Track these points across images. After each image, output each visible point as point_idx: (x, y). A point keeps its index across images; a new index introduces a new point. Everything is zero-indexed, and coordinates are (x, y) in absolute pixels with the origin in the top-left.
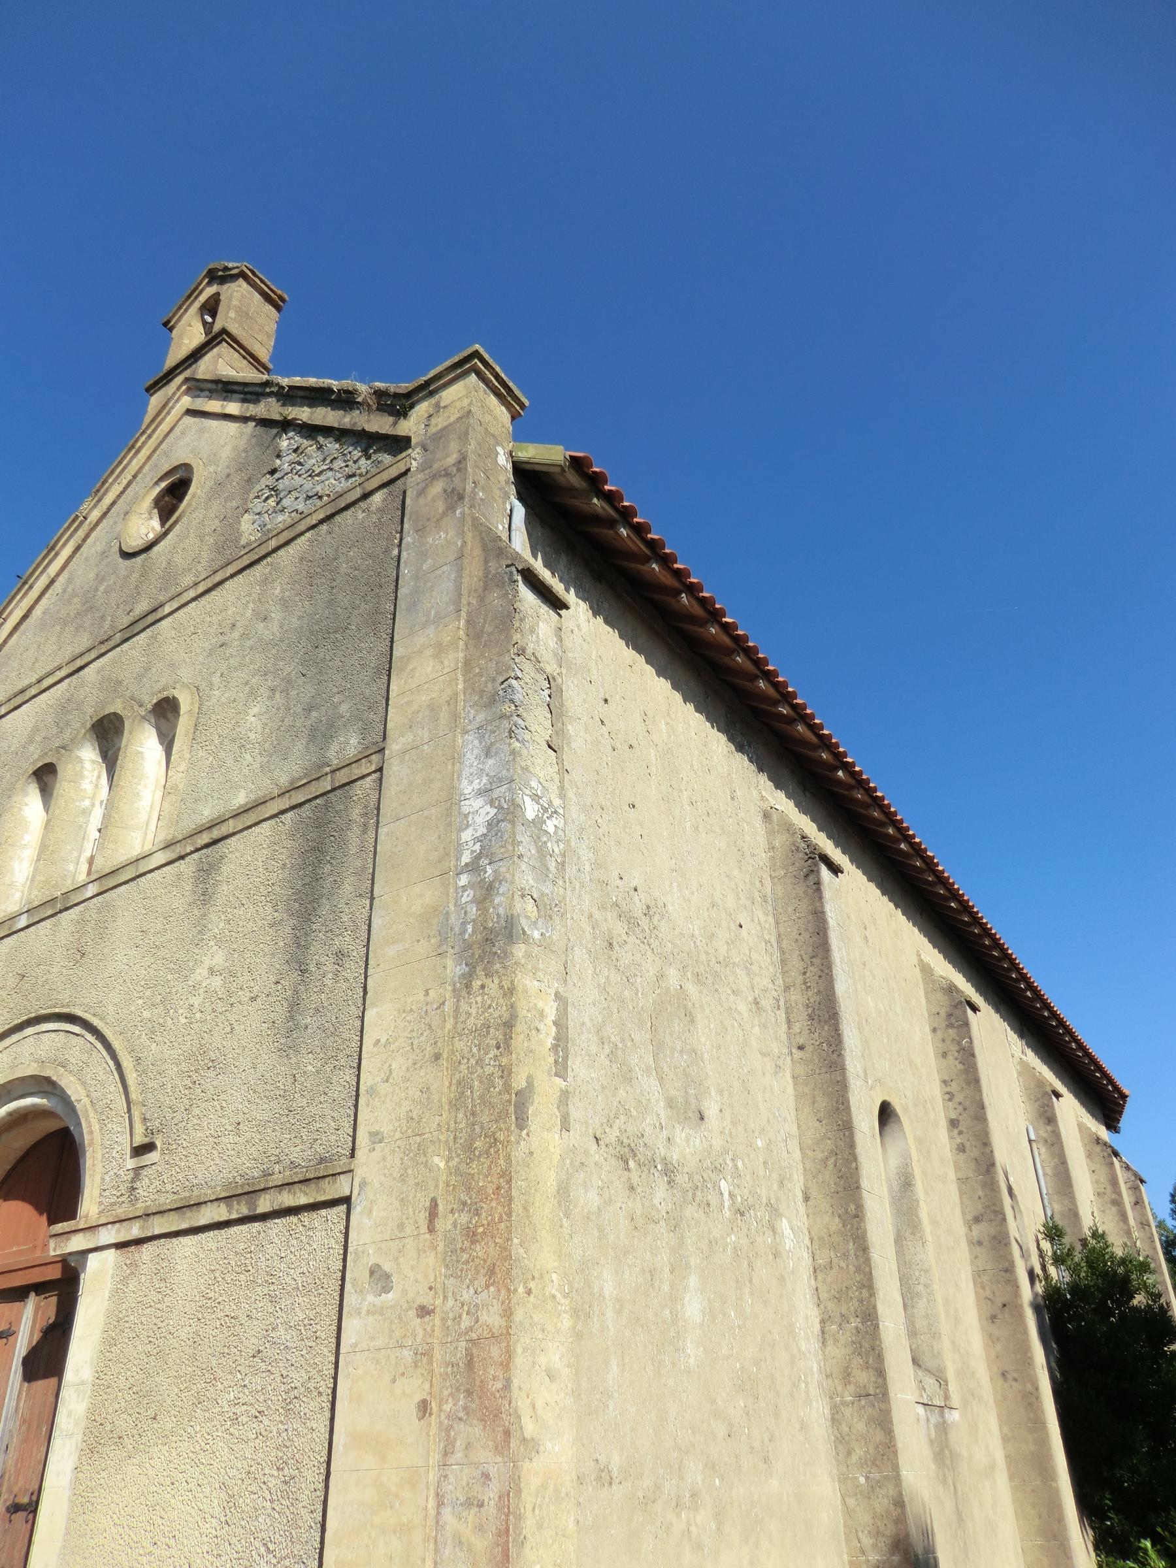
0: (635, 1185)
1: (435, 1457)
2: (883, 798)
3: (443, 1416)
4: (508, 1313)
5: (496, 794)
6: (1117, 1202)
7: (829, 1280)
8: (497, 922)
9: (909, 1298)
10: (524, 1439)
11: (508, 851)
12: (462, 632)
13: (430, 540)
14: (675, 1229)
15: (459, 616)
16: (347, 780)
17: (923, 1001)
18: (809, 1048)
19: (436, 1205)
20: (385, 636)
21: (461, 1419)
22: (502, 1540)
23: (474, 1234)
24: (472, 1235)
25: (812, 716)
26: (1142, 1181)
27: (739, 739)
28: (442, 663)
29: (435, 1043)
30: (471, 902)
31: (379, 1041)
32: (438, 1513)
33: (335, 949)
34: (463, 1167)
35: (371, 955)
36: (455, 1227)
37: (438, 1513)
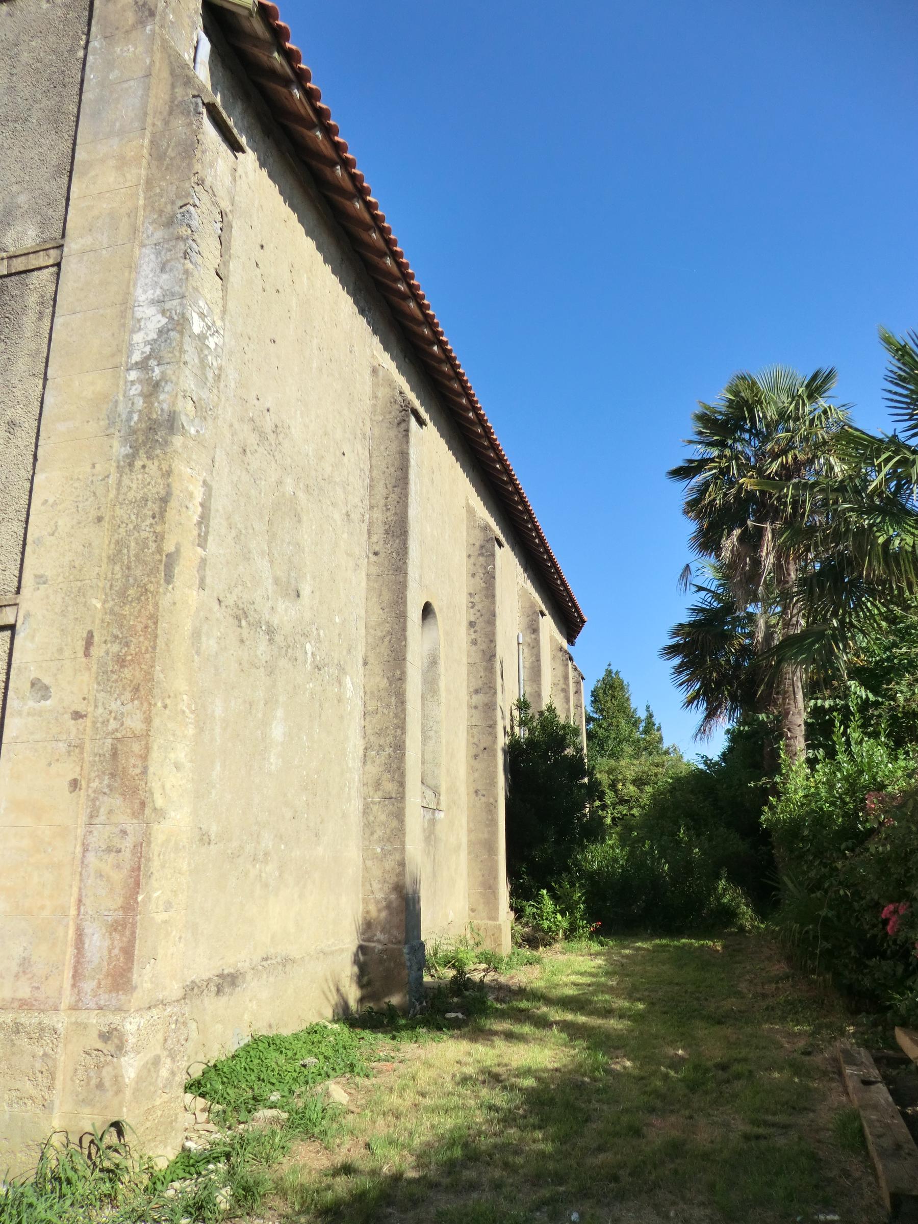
0: (245, 639)
1: (83, 819)
2: (463, 375)
3: (90, 791)
4: (148, 721)
5: (168, 306)
6: (565, 691)
7: (374, 721)
8: (161, 415)
9: (425, 738)
10: (155, 809)
11: (175, 356)
12: (145, 151)
13: (118, 50)
14: (270, 674)
15: (144, 134)
16: (22, 268)
17: (465, 534)
18: (382, 555)
19: (92, 636)
20: (66, 137)
21: (105, 793)
22: (134, 874)
23: (123, 661)
24: (121, 662)
25: (423, 297)
26: (583, 678)
27: (362, 304)
28: (124, 176)
29: (99, 508)
30: (139, 395)
31: (46, 501)
32: (84, 856)
33: (7, 419)
34: (117, 609)
35: (42, 429)
36: (107, 654)
37: (84, 856)
